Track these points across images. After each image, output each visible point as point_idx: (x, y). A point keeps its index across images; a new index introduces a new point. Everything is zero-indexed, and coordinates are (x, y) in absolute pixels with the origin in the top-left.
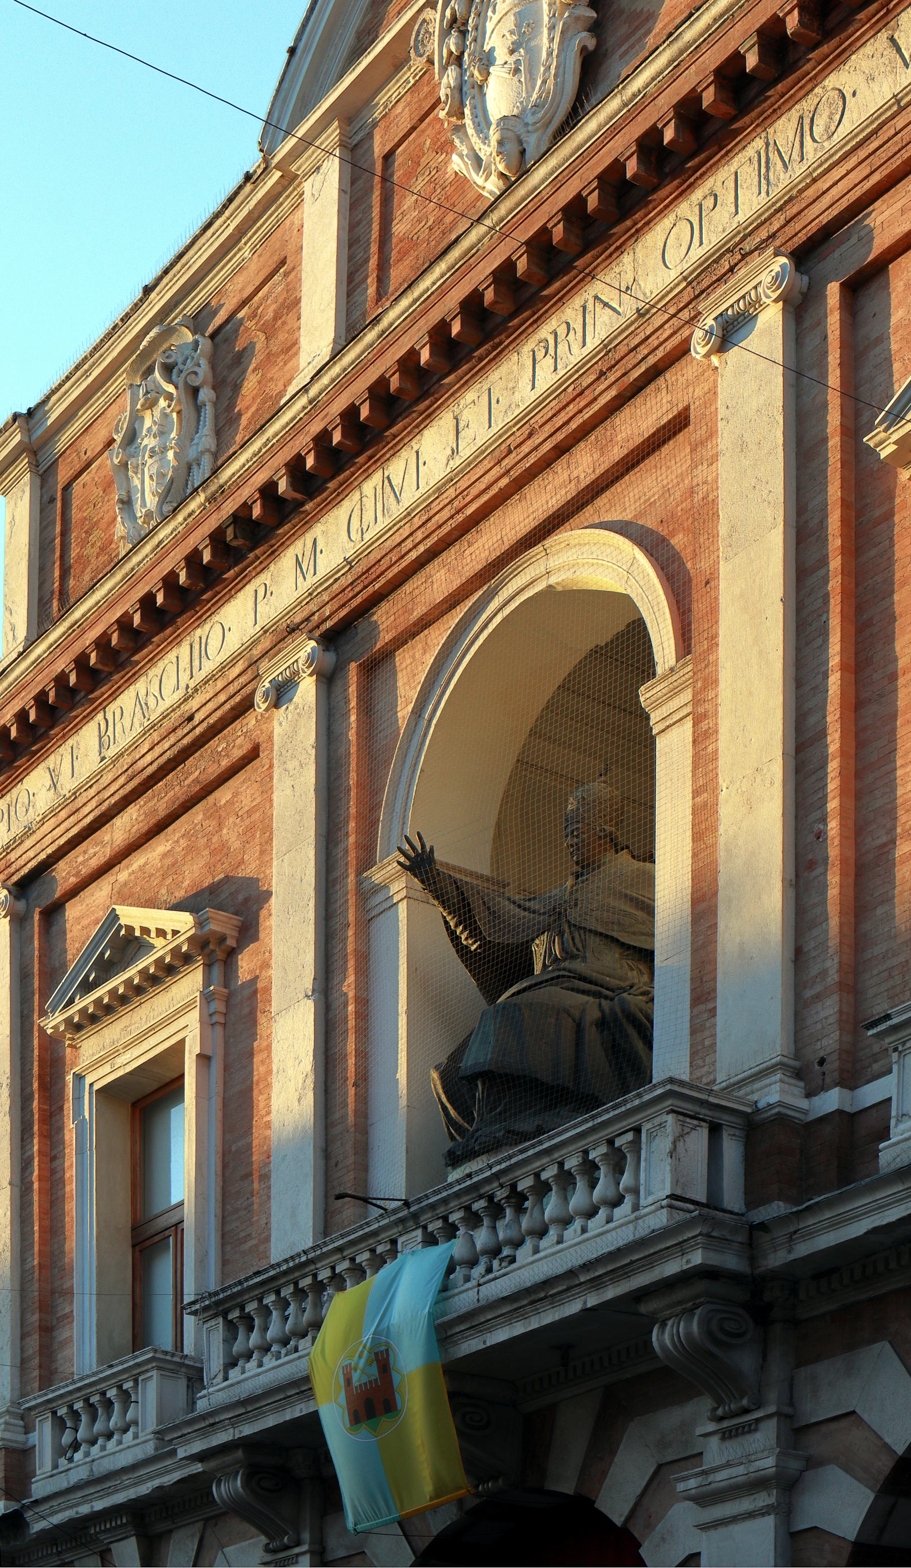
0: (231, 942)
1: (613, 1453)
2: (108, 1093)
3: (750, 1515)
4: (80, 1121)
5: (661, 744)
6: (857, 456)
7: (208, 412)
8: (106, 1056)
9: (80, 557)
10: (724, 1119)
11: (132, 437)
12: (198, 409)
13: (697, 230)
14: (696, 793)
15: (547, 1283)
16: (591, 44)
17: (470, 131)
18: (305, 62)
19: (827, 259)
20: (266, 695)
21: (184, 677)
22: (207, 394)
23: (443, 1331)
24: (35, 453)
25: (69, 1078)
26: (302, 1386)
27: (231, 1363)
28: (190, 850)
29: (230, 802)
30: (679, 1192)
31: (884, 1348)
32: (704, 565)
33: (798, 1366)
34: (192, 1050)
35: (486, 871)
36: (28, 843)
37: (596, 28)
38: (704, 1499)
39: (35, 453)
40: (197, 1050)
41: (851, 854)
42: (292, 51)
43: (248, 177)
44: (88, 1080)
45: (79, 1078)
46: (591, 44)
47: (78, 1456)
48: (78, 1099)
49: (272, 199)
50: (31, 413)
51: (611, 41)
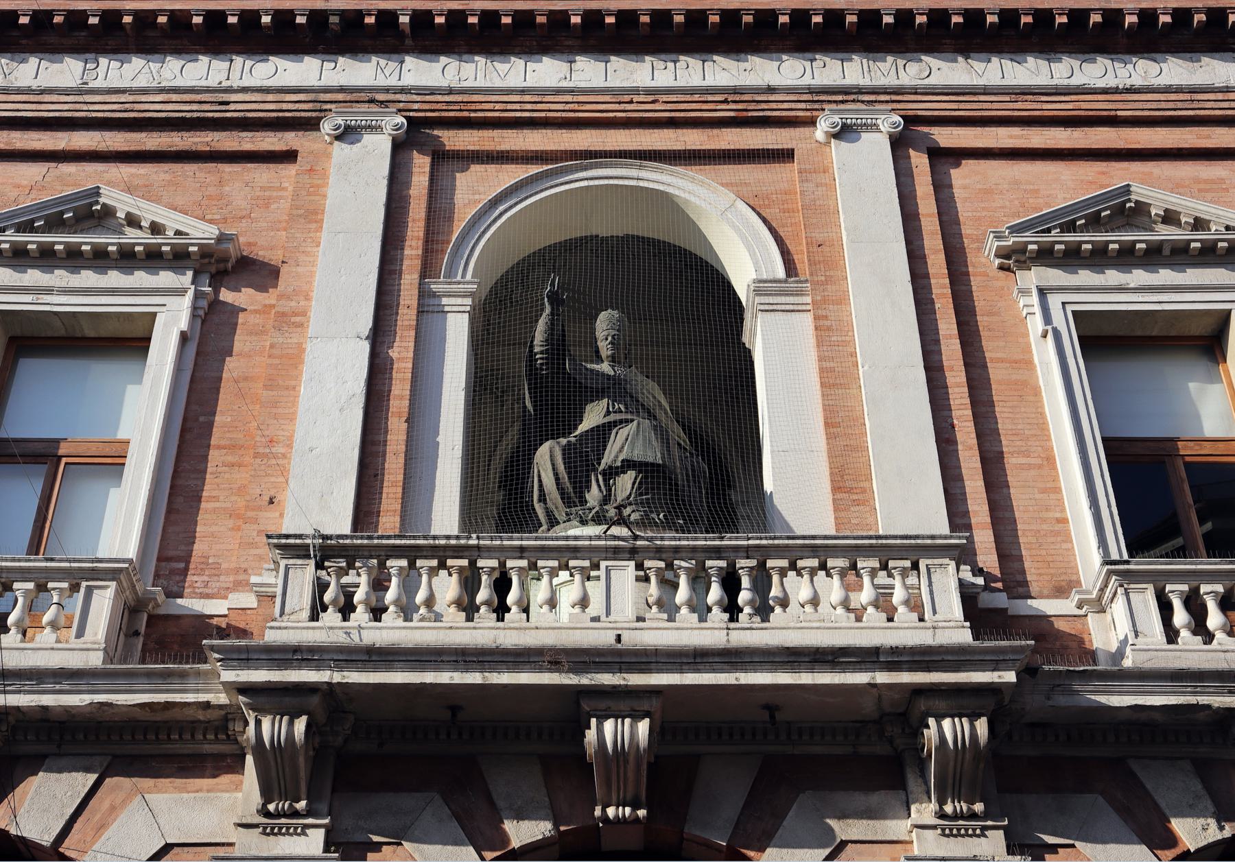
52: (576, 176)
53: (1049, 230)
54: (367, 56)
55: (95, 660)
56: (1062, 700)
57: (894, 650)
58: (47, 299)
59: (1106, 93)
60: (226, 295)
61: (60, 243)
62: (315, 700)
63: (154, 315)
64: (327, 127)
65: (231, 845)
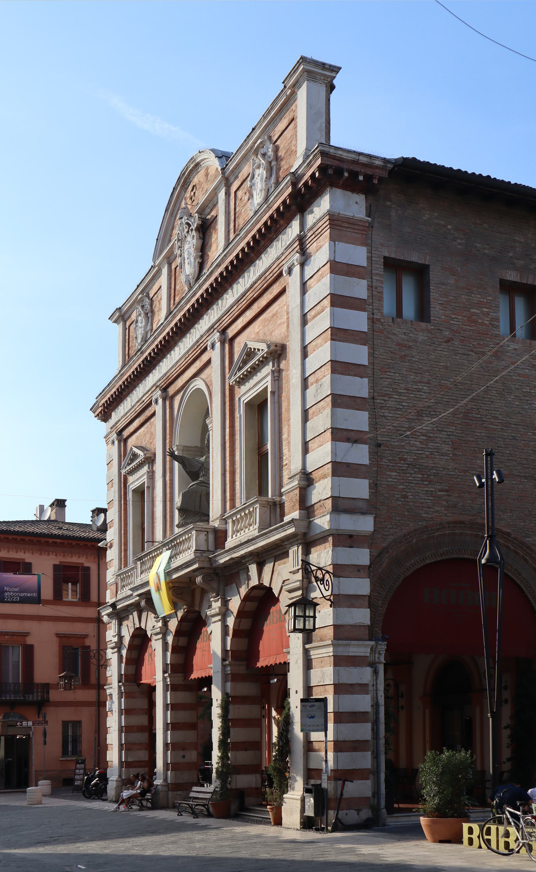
2: (134, 491)
3: (217, 621)
10: (208, 530)
11: (137, 322)
20: (286, 271)
23: (168, 574)
24: (123, 316)
26: (147, 583)
27: (141, 573)
28: (147, 431)
30: (197, 549)
33: (226, 586)
34: (269, 390)
36: (120, 422)
42: (157, 240)
43: (152, 266)
44: (242, 400)
46: (200, 261)
50: (120, 308)
56: (217, 564)
58: (136, 483)
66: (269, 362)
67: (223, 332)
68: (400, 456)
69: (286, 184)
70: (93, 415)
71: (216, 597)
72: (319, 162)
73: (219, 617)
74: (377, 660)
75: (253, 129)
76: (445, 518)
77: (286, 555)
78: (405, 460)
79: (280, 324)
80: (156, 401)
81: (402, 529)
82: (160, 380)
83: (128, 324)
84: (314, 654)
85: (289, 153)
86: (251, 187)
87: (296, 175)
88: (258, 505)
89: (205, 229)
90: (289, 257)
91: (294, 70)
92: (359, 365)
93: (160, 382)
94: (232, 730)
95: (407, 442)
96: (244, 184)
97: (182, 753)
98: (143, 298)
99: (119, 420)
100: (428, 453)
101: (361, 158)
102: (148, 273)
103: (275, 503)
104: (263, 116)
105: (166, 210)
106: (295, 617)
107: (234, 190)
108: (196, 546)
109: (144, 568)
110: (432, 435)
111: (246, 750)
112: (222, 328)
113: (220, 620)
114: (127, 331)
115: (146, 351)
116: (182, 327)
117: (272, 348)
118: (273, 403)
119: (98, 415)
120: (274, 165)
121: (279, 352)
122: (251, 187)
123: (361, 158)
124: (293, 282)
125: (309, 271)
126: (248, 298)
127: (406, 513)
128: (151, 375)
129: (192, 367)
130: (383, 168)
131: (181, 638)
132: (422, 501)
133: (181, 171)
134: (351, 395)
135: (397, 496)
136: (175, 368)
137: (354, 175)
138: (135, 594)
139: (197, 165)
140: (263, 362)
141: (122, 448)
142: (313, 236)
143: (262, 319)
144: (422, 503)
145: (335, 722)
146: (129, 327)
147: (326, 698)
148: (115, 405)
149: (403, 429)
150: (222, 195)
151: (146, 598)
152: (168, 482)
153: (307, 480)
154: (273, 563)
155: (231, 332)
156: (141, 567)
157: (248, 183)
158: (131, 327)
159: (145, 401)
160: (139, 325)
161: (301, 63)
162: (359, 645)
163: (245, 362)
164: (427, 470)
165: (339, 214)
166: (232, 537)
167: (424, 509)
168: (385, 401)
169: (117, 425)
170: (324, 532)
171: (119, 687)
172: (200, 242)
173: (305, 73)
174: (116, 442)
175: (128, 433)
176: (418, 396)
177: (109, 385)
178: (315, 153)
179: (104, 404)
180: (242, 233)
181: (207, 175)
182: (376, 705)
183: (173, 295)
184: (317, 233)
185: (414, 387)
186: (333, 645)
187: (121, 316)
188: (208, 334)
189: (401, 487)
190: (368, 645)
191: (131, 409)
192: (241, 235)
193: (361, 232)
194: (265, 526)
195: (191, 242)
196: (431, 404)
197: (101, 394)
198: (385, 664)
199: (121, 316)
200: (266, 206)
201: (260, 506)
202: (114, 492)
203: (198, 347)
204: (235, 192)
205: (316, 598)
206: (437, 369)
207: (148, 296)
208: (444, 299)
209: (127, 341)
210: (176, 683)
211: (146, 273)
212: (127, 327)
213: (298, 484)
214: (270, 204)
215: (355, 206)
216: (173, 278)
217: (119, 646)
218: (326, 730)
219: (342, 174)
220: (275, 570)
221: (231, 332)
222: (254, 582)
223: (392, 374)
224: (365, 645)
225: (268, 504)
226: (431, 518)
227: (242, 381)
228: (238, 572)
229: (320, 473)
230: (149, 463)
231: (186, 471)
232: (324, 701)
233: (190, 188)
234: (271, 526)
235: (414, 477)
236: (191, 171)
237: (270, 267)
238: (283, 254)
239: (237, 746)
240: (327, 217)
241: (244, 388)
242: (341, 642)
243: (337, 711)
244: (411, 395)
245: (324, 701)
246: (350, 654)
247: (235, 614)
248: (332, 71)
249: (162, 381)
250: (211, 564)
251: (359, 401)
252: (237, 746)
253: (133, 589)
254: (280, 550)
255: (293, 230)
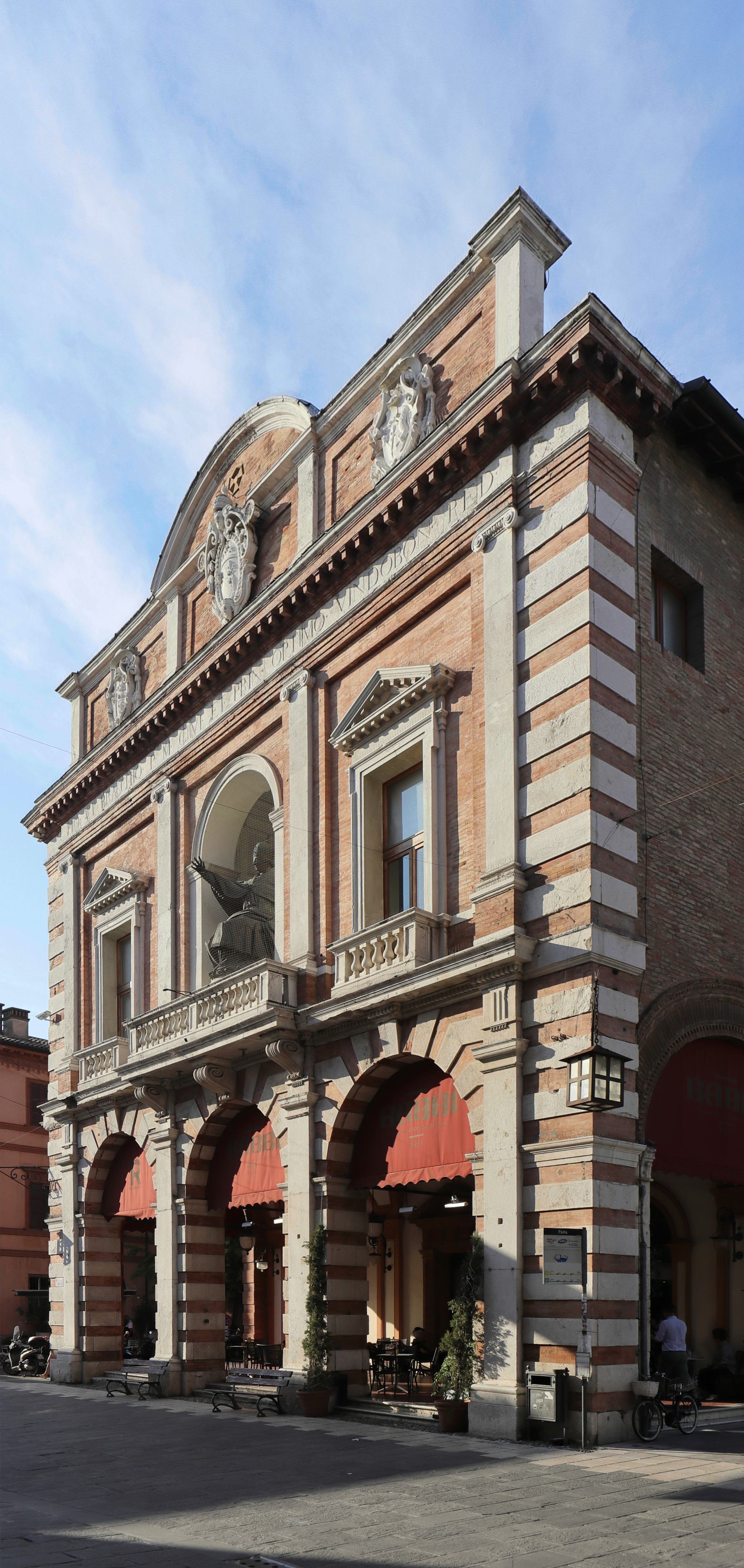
0: (146, 885)
1: (263, 1088)
2: (106, 936)
3: (301, 1116)
4: (97, 945)
5: (276, 834)
6: (329, 747)
7: (138, 684)
8: (105, 924)
9: (97, 730)
10: (288, 973)
11: (113, 689)
12: (135, 683)
13: (282, 655)
14: (285, 855)
15: (232, 1028)
16: (254, 577)
17: (217, 599)
18: (166, 561)
19: (179, 782)
20: (480, 542)
21: (129, 784)
22: (137, 678)
24: (81, 688)
25: (93, 930)
27: (139, 1046)
28: (133, 848)
29: (146, 833)
31: (339, 1058)
32: (286, 773)
35: (232, 868)
36: (79, 838)
37: (256, 571)
38: (289, 1108)
39: (81, 688)
40: (432, 744)
41: (330, 883)
42: (161, 556)
43: (148, 600)
44: (99, 931)
45: (96, 930)
46: (254, 577)
47: (93, 1076)
48: (96, 937)
49: (157, 610)
50: (78, 673)
51: (261, 577)
52: (226, 776)
53: (350, 727)
54: (330, 602)
55: (411, 967)
56: (310, 1023)
57: (243, 1023)
58: (110, 925)
59: (387, 588)
60: (454, 708)
61: (402, 699)
62: (143, 1081)
63: (421, 741)
64: (475, 548)
65: (482, 1042)
66: (428, 701)
67: (315, 670)
68: (670, 864)
69: (501, 381)
70: (26, 830)
71: (299, 1078)
72: (585, 330)
73: (306, 1110)
74: (642, 1175)
75: (389, 341)
76: (720, 973)
77: (476, 1003)
78: (676, 872)
79: (450, 642)
80: (159, 798)
81: (672, 978)
82: (168, 762)
83: (90, 699)
84: (540, 1160)
85: (467, 372)
86: (378, 438)
87: (524, 366)
88: (414, 923)
89: (266, 526)
90: (492, 514)
91: (500, 216)
92: (624, 699)
93: (168, 766)
94: (329, 1282)
95: (679, 845)
96: (354, 445)
97: (204, 1316)
98: (129, 651)
99: (78, 834)
100: (702, 870)
101: (643, 355)
102: (139, 612)
103: (439, 925)
104: (414, 314)
105: (181, 510)
106: (594, 1076)
107: (333, 457)
108: (270, 995)
109: (144, 1038)
110: (706, 844)
111: (349, 1314)
112: (312, 665)
113: (306, 1114)
114: (89, 709)
115: (142, 717)
116: (224, 671)
117: (442, 673)
118: (436, 766)
119: (35, 830)
120: (435, 396)
121: (449, 684)
122: (378, 438)
123: (643, 355)
124: (493, 570)
125: (531, 538)
126: (378, 606)
127: (677, 955)
128: (148, 758)
129: (236, 738)
130: (668, 391)
131: (204, 1147)
132: (695, 941)
133: (215, 443)
134: (616, 744)
135: (667, 925)
136: (200, 742)
137: (630, 381)
138: (124, 1078)
139: (249, 432)
140: (413, 704)
141: (82, 877)
142: (547, 478)
143: (404, 641)
144: (695, 944)
145: (594, 1271)
146: (93, 704)
147: (584, 1229)
148: (69, 812)
149: (674, 824)
150: (307, 465)
151: (146, 1085)
152: (182, 916)
153: (531, 879)
154: (432, 1023)
155: (331, 670)
156: (138, 1038)
157: (374, 431)
158: (96, 704)
159: (134, 800)
160: (118, 692)
161: (516, 201)
162: (626, 1148)
163: (370, 708)
164: (700, 896)
165: (603, 441)
166: (347, 980)
167: (698, 954)
168: (654, 771)
169: (73, 842)
170: (574, 958)
171: (77, 1220)
172: (254, 549)
173: (520, 225)
174: (70, 868)
175: (95, 854)
176: (691, 780)
177: (62, 778)
178: (577, 315)
179: (49, 811)
180: (381, 488)
181: (269, 445)
182: (642, 1245)
183: (189, 641)
184: (554, 472)
185: (687, 763)
186: (595, 1144)
187: (80, 687)
188: (279, 678)
189: (671, 912)
190: (637, 1150)
191: (102, 816)
192: (377, 492)
193: (627, 487)
194: (427, 957)
195: (238, 548)
196: (706, 798)
197: (45, 794)
198: (652, 1183)
199: (80, 687)
200: (446, 429)
201: (417, 925)
202: (66, 940)
203: (255, 701)
204: (335, 460)
205: (550, 1068)
206: (712, 748)
207: (134, 650)
208: (719, 646)
209: (89, 723)
210: (194, 1213)
211: (135, 612)
212: (89, 704)
213: (514, 882)
214: (454, 426)
215: (621, 441)
216: (190, 616)
217: (77, 1158)
218: (584, 1283)
219: (613, 375)
220: (438, 1030)
221: (331, 670)
222: (391, 1050)
223: (661, 733)
224: (634, 1149)
225: (429, 924)
226: (706, 969)
227: (353, 744)
228: (348, 1039)
229: (559, 865)
230: (139, 894)
231: (219, 899)
232: (582, 1233)
233: (230, 473)
234: (431, 960)
235: (687, 902)
236: (235, 442)
237: (437, 545)
238: (469, 518)
239: (333, 1307)
240: (587, 439)
241: (360, 753)
242: (607, 1140)
243: (597, 1252)
244: (683, 775)
245: (582, 1233)
246: (614, 1162)
247: (339, 1106)
248: (559, 241)
249: (172, 764)
250: (296, 1025)
251: (624, 757)
252: (333, 1307)
253: (121, 1071)
254: (457, 996)
255: (502, 470)
